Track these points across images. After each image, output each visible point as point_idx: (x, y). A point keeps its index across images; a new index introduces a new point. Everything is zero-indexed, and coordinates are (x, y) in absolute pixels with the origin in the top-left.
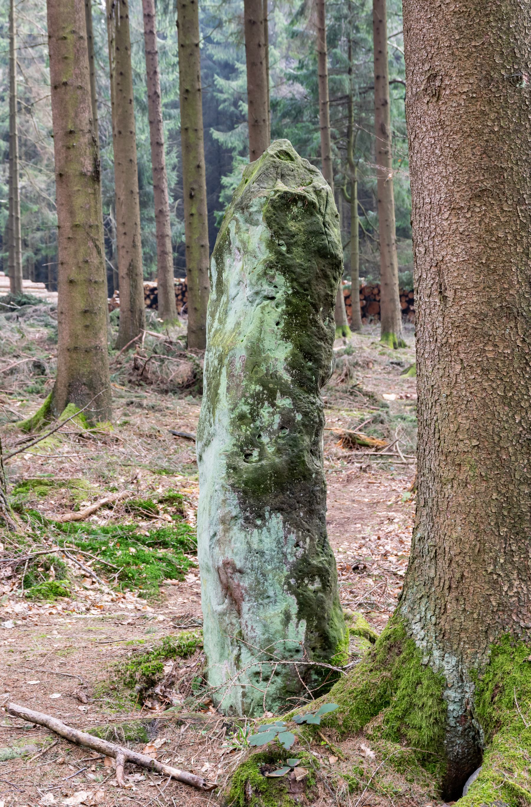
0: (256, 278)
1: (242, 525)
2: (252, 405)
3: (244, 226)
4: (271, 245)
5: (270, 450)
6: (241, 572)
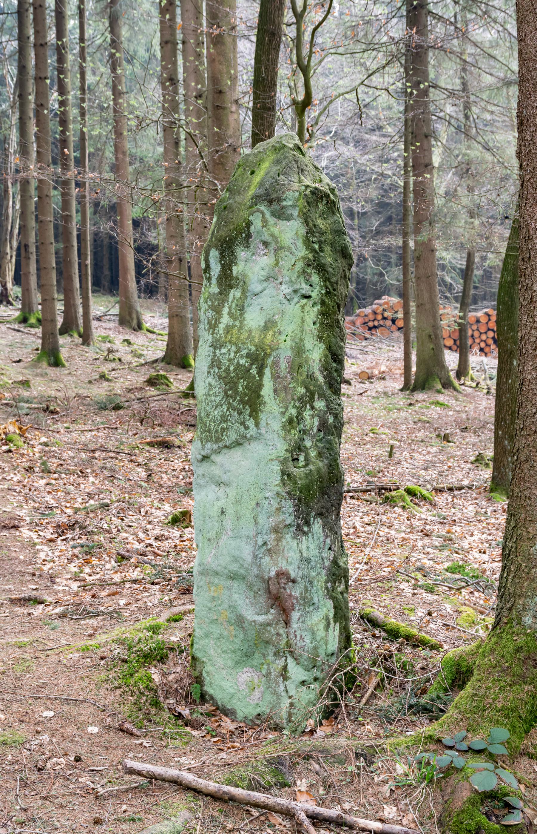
0: (295, 275)
1: (294, 534)
2: (298, 408)
3: (271, 220)
4: (307, 242)
5: (313, 454)
6: (294, 581)
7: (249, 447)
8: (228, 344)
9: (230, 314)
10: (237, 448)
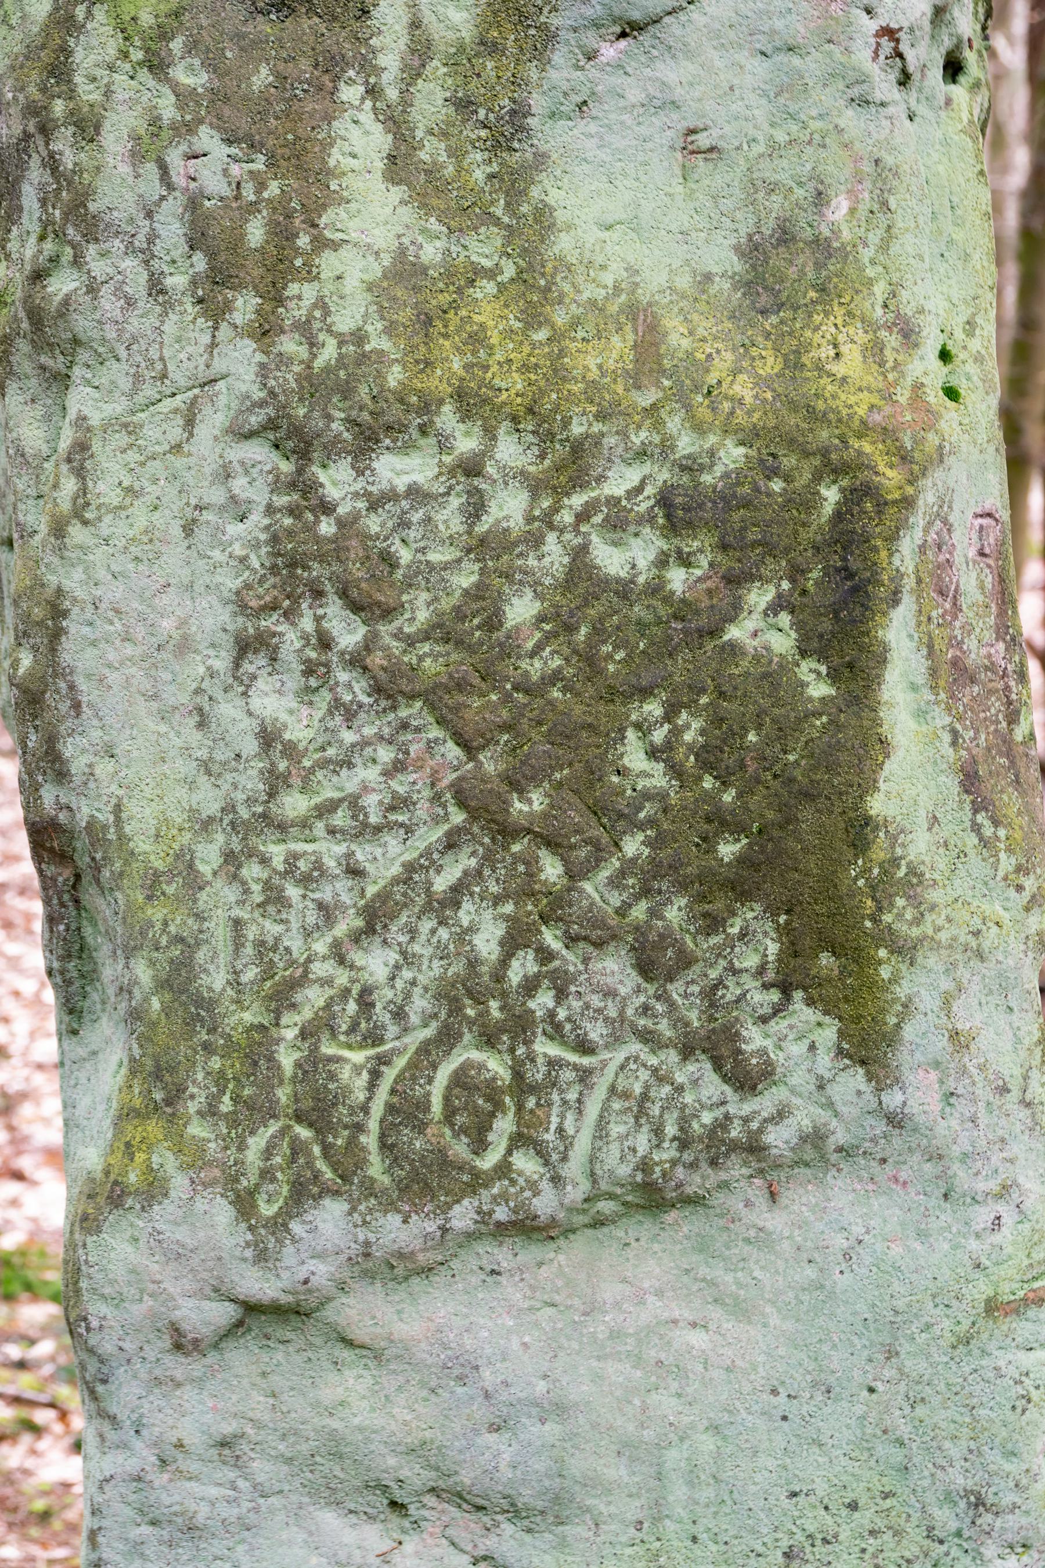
7: (775, 1221)
8: (447, 418)
9: (398, 165)
10: (638, 1228)
